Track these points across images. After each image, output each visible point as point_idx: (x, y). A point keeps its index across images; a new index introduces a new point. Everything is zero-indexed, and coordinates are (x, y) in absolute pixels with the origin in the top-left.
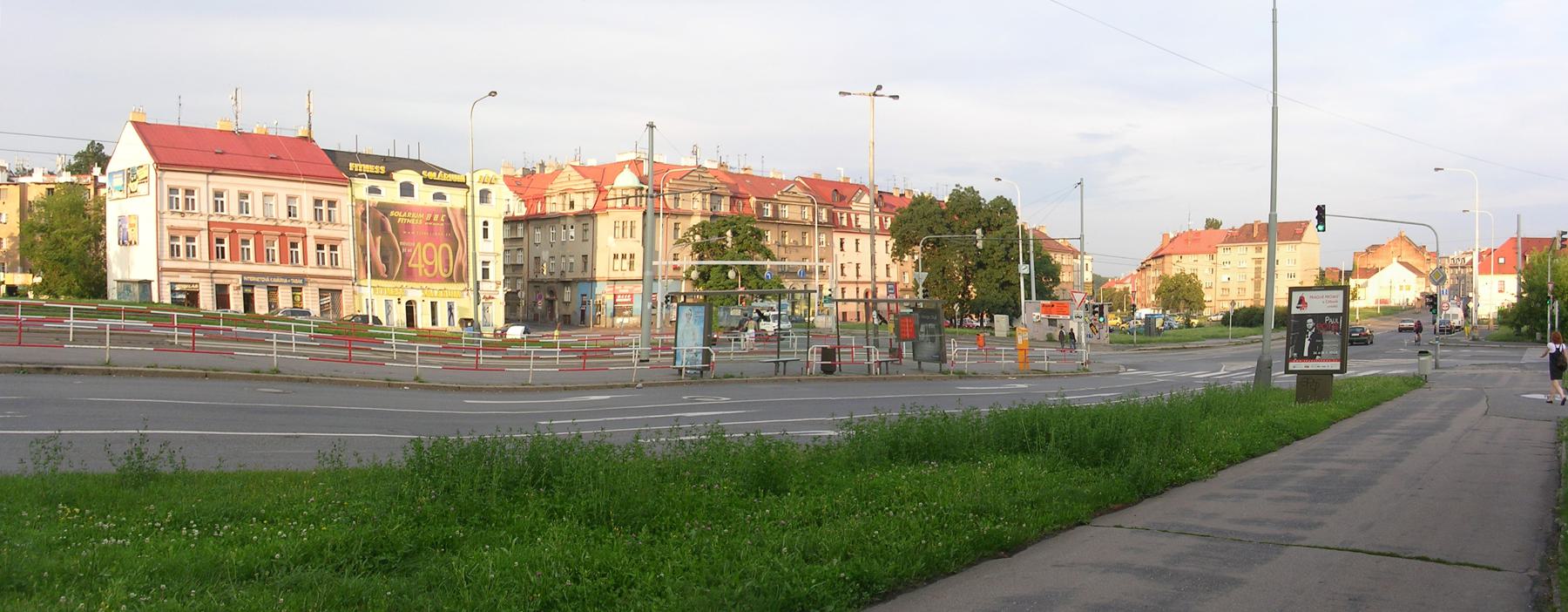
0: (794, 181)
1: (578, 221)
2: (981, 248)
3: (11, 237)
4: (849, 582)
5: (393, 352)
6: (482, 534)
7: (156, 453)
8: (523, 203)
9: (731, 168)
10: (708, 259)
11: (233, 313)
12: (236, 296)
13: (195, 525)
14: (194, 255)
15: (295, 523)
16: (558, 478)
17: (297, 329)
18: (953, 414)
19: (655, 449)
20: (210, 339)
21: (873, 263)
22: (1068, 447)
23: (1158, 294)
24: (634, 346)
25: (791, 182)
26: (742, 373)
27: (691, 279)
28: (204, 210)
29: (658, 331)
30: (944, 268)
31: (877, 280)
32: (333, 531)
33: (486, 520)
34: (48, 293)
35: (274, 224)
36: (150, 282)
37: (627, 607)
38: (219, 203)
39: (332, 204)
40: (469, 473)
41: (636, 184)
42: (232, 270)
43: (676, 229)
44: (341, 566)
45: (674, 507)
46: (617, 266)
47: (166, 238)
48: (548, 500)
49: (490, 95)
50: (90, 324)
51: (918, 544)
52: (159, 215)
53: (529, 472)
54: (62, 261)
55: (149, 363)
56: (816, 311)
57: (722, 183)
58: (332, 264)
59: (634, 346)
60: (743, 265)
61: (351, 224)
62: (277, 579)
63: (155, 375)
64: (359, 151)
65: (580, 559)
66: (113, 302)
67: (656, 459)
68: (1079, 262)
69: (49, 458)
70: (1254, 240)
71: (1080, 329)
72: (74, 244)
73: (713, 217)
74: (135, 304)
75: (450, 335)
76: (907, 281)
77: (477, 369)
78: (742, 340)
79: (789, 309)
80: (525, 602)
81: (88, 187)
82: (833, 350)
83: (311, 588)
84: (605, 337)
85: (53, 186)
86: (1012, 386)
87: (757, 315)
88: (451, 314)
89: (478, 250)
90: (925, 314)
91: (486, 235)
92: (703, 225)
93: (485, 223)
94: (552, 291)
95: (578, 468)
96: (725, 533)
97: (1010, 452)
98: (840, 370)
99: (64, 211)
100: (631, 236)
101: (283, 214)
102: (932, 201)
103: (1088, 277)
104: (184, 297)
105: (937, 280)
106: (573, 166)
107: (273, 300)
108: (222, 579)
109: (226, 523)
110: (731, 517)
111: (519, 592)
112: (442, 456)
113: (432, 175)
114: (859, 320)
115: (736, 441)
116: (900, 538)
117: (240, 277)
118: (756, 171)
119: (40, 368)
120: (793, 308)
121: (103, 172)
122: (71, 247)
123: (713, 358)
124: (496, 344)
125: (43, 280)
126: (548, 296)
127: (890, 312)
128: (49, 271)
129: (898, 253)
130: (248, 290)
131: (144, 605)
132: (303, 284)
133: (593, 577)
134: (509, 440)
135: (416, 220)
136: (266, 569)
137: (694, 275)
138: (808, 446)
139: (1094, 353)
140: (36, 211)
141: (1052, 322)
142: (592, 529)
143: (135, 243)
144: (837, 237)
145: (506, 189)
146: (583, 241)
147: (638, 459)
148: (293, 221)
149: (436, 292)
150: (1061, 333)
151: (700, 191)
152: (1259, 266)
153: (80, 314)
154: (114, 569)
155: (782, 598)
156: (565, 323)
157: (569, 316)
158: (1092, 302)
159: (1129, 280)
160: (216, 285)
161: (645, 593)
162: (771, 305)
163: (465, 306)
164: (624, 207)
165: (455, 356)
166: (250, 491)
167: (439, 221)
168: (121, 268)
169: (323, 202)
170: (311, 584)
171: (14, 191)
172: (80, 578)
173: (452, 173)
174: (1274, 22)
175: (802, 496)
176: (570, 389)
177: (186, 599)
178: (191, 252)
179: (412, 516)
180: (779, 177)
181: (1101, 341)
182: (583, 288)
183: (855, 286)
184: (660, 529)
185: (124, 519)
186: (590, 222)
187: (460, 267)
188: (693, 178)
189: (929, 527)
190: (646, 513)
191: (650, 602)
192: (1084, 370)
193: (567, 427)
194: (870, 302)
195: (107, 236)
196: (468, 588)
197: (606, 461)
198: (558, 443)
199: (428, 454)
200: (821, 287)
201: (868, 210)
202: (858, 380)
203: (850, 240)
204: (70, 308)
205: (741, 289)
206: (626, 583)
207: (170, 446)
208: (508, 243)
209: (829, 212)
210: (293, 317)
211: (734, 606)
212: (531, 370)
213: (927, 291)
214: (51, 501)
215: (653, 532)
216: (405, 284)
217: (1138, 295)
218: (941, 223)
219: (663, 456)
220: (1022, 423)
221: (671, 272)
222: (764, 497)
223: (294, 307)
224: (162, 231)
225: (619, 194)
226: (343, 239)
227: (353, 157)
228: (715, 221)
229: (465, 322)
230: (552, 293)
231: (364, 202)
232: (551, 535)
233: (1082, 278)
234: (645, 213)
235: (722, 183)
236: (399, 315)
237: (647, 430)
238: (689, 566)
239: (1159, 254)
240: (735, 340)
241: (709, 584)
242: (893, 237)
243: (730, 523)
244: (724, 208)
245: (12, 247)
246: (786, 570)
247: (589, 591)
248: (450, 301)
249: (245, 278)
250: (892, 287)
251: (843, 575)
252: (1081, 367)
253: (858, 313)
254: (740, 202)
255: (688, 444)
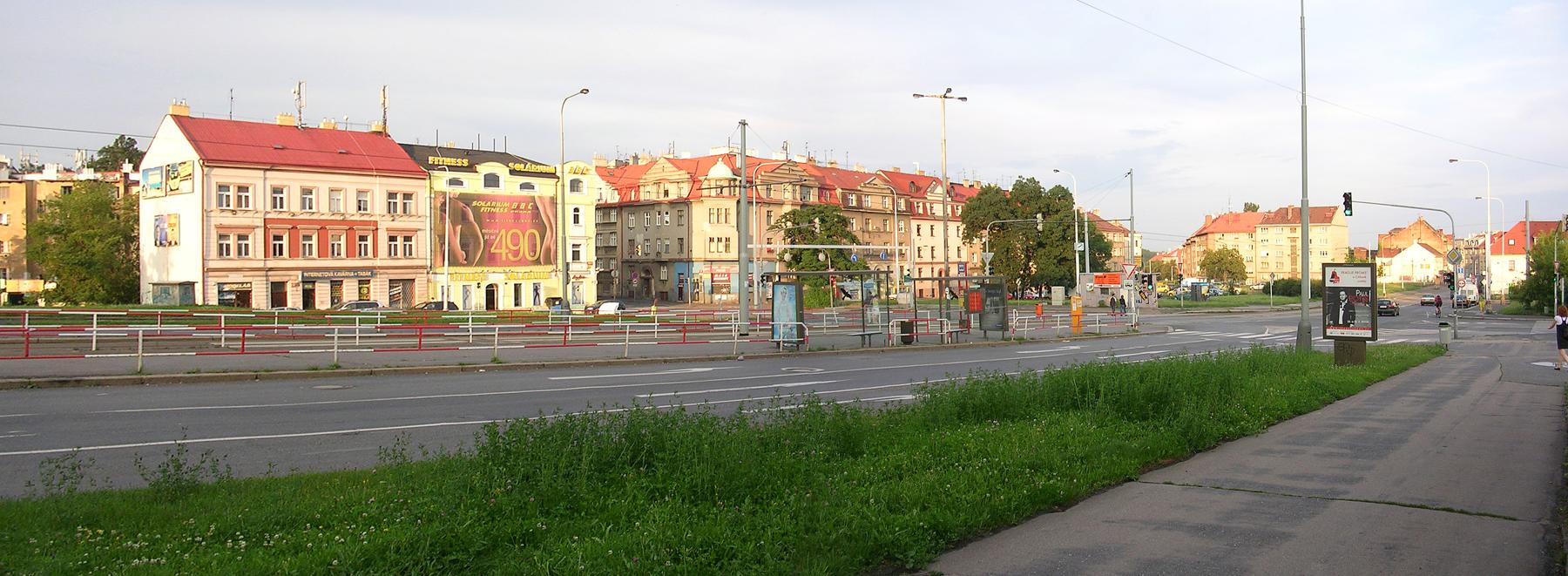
2: (1041, 230)
3: (15, 240)
4: (927, 530)
6: (569, 524)
7: (197, 463)
8: (616, 192)
10: (799, 243)
11: (289, 311)
13: (242, 537)
14: (247, 254)
16: (660, 455)
18: (1012, 377)
19: (757, 420)
20: (263, 338)
21: (946, 246)
22: (1116, 402)
23: (1202, 266)
28: (260, 207)
29: (755, 308)
32: (396, 533)
34: (64, 300)
35: (342, 218)
36: (193, 284)
39: (407, 196)
41: (730, 175)
42: (291, 267)
43: (769, 216)
44: (407, 568)
45: (775, 475)
49: (582, 92)
52: (206, 213)
54: (82, 265)
55: (190, 369)
57: (811, 176)
58: (405, 254)
61: (428, 215)
65: (682, 539)
67: (759, 430)
68: (1129, 239)
69: (65, 478)
70: (1288, 222)
71: (1129, 295)
72: (98, 247)
74: (175, 307)
76: (975, 261)
77: (565, 345)
81: (117, 185)
82: (911, 323)
85: (71, 184)
86: (1066, 348)
90: (990, 289)
92: (794, 213)
93: (576, 210)
94: (648, 270)
97: (1062, 409)
99: (86, 210)
101: (353, 208)
102: (998, 191)
103: (1138, 251)
105: (1002, 258)
107: (337, 295)
109: (277, 532)
113: (519, 167)
114: (933, 296)
116: (969, 491)
120: (879, 287)
121: (136, 169)
122: (95, 250)
123: (807, 332)
125: (58, 286)
126: (643, 275)
127: (960, 288)
128: (65, 276)
129: (968, 237)
132: (372, 277)
134: (603, 416)
137: (787, 257)
139: (1143, 316)
140: (48, 211)
141: (1104, 291)
142: (696, 506)
143: (176, 243)
144: (914, 224)
145: (598, 178)
148: (363, 215)
149: (521, 275)
150: (1113, 299)
152: (1294, 244)
153: (103, 320)
158: (1142, 273)
159: (1175, 254)
160: (272, 283)
163: (553, 285)
165: (540, 334)
167: (526, 208)
169: (398, 195)
171: (19, 191)
173: (541, 164)
174: (1302, 29)
178: (243, 251)
181: (1150, 305)
182: (679, 268)
183: (930, 266)
184: (762, 499)
185: (159, 536)
187: (548, 250)
188: (784, 171)
189: (991, 480)
190: (750, 484)
191: (749, 570)
192: (1134, 331)
193: (669, 400)
194: (943, 280)
195: (141, 236)
197: (711, 434)
201: (942, 199)
202: (933, 349)
203: (925, 226)
204: (93, 315)
206: (727, 556)
207: (213, 455)
209: (906, 201)
214: (68, 524)
215: (756, 502)
216: (485, 269)
217: (1184, 267)
220: (1073, 381)
224: (208, 230)
225: (713, 185)
227: (433, 150)
229: (551, 301)
230: (647, 272)
231: (444, 194)
232: (652, 518)
233: (1132, 252)
234: (738, 202)
235: (811, 176)
236: (478, 299)
239: (1205, 231)
242: (963, 223)
244: (813, 198)
247: (690, 569)
248: (536, 281)
249: (305, 274)
250: (963, 266)
252: (1131, 329)
253: (933, 290)
255: (788, 413)
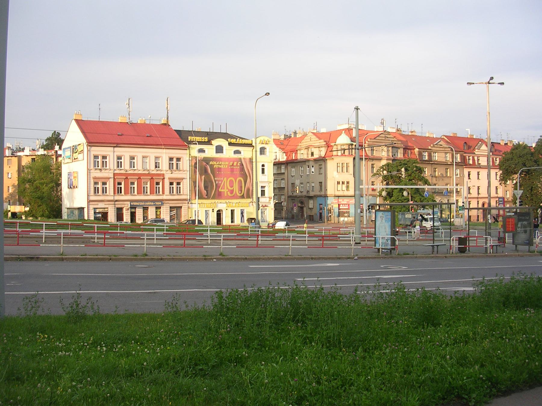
0: (441, 138)
1: (316, 163)
3: (13, 186)
5: (208, 239)
6: (259, 354)
7: (85, 304)
8: (284, 154)
9: (404, 131)
10: (391, 184)
12: (127, 214)
13: (104, 345)
14: (106, 192)
15: (153, 344)
16: (309, 317)
17: (157, 230)
24: (351, 234)
25: (439, 139)
26: (413, 252)
27: (382, 196)
28: (112, 168)
29: (365, 226)
30: (532, 188)
31: (491, 196)
33: (262, 345)
35: (148, 172)
37: (348, 398)
38: (120, 163)
39: (178, 159)
40: (251, 313)
41: (349, 142)
43: (373, 167)
44: (178, 371)
45: (377, 335)
46: (339, 188)
47: (92, 183)
48: (303, 331)
49: (266, 95)
50: (53, 233)
51: (523, 362)
52: (89, 170)
53: (291, 311)
54: (39, 198)
55: (82, 253)
56: (455, 215)
57: (398, 140)
58: (177, 193)
59: (351, 234)
60: (412, 188)
61: (188, 170)
62: (146, 377)
63: (85, 260)
64: (193, 130)
65: (322, 370)
66: (65, 220)
69: (32, 307)
72: (45, 189)
73: (394, 160)
74: (76, 221)
75: (241, 228)
76: (508, 196)
77: (257, 247)
78: (413, 232)
79: (439, 214)
80: (287, 397)
81: (53, 157)
83: (163, 383)
84: (335, 228)
85: (34, 157)
87: (420, 218)
88: (242, 216)
89: (259, 180)
90: (521, 216)
91: (263, 172)
92: (388, 165)
93: (263, 166)
94: (302, 202)
95: (322, 310)
96: (405, 351)
98: (469, 251)
99: (40, 170)
100: (347, 171)
101: (153, 167)
102: (525, 147)
104: (100, 215)
106: (312, 132)
107: (145, 215)
108: (118, 376)
109: (119, 344)
110: (409, 341)
111: (283, 391)
112: (234, 302)
113: (233, 141)
114: (478, 220)
115: (411, 294)
116: (513, 357)
117: (129, 203)
118: (419, 132)
119: (29, 257)
120: (441, 214)
121: (60, 148)
122: (44, 191)
123: (397, 243)
124: (269, 232)
125: (30, 209)
126: (299, 205)
129: (504, 179)
130: (133, 210)
131: (80, 390)
133: (328, 381)
135: (224, 165)
136: (140, 371)
137: (384, 194)
138: (451, 297)
140: (26, 171)
142: (330, 350)
143: (76, 187)
144: (466, 171)
146: (319, 174)
147: (357, 304)
149: (234, 204)
151: (386, 146)
153: (48, 227)
154: (64, 369)
155: (446, 385)
156: (310, 220)
157: (313, 216)
160: (117, 208)
161: (359, 389)
162: (429, 212)
163: (251, 211)
164: (342, 155)
165: (244, 240)
166: (131, 325)
167: (237, 165)
168: (69, 201)
169: (174, 159)
170: (163, 381)
171: (15, 160)
172: (47, 373)
175: (448, 327)
176: (315, 259)
177: (100, 387)
178: (104, 191)
179: (216, 342)
180: (432, 136)
182: (320, 200)
183: (476, 200)
184: (369, 349)
185: (69, 341)
186: (323, 164)
187: (248, 189)
190: (362, 339)
193: (314, 282)
194: (486, 210)
196: (252, 388)
197: (338, 305)
198: (309, 293)
199: (226, 301)
200: (457, 201)
202: (480, 257)
203: (474, 172)
204: (43, 224)
205: (411, 202)
206: (348, 383)
208: (276, 176)
209: (461, 156)
210: (156, 224)
211: (419, 387)
212: (291, 247)
213: (522, 202)
214: (33, 331)
215: (365, 351)
216: (216, 201)
218: (531, 160)
219: (371, 302)
221: (370, 192)
222: (427, 328)
223: (156, 218)
224: (90, 180)
225: (339, 148)
226: (184, 178)
228: (395, 163)
229: (250, 220)
230: (302, 203)
231: (196, 157)
232: (305, 355)
234: (354, 159)
235: (398, 140)
236: (213, 218)
237: (361, 286)
238: (385, 371)
240: (409, 232)
241: (405, 372)
242: (500, 169)
243: (408, 344)
244: (400, 155)
245: (14, 191)
246: (449, 369)
249: (132, 204)
250: (502, 200)
251: (481, 376)
253: (478, 216)
254: (409, 151)
255: (385, 295)
